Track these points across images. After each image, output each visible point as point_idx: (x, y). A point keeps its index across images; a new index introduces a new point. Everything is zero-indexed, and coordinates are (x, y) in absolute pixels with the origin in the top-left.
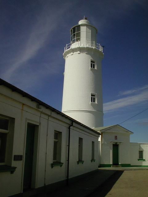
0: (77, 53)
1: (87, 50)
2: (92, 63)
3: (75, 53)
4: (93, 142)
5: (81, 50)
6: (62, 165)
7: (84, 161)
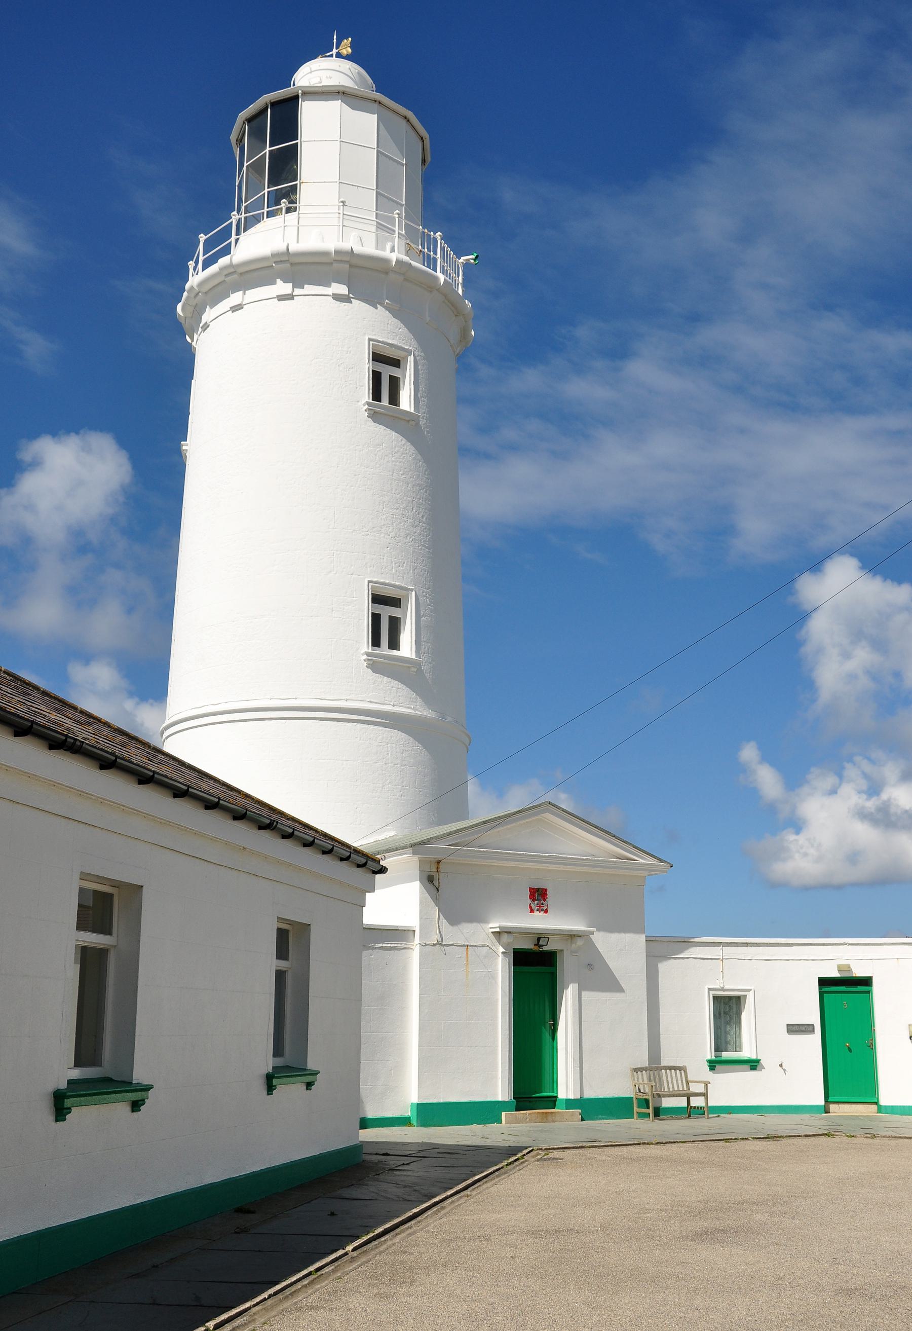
0: (329, 291)
1: (358, 276)
2: (381, 367)
3: (309, 289)
4: (289, 939)
5: (300, 269)
6: (308, 1079)
7: (316, 1073)
